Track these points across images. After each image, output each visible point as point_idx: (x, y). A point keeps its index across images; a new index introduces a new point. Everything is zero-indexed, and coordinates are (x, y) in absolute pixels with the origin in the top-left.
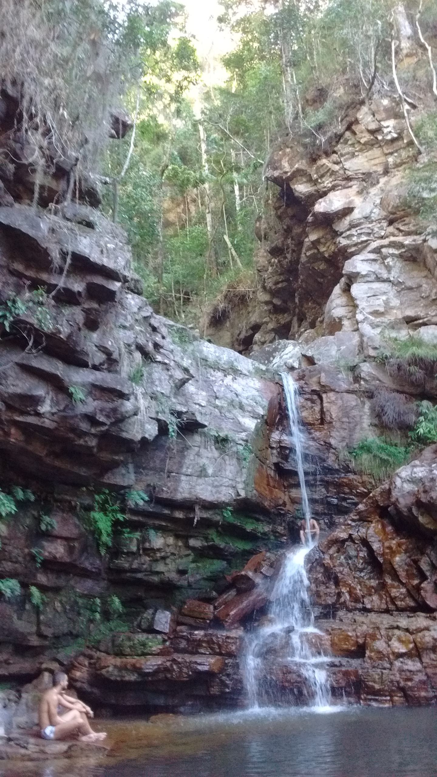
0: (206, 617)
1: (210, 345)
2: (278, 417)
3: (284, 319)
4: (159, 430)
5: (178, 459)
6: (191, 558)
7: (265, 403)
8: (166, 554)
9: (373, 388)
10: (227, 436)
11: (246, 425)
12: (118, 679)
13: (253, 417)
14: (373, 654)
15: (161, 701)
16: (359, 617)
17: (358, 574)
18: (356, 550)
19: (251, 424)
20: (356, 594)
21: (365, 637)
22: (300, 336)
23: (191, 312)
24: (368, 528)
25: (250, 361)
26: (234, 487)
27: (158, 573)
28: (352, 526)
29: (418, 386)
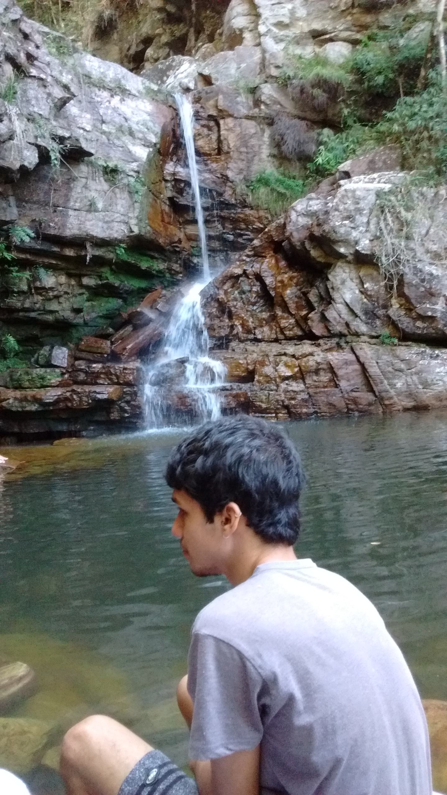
0: (103, 351)
1: (93, 58)
2: (172, 146)
3: (179, 30)
4: (39, 157)
5: (63, 191)
6: (85, 297)
7: (158, 129)
8: (57, 292)
9: (274, 113)
10: (116, 166)
11: (137, 155)
12: (20, 409)
13: (144, 145)
14: (261, 378)
15: (64, 428)
16: (250, 347)
17: (251, 308)
18: (250, 285)
19: (142, 153)
20: (248, 326)
21: (255, 364)
22: (197, 51)
23: (71, 21)
24: (262, 263)
25: (140, 79)
26: (127, 223)
27: (52, 312)
28: (247, 262)
29: (321, 112)
